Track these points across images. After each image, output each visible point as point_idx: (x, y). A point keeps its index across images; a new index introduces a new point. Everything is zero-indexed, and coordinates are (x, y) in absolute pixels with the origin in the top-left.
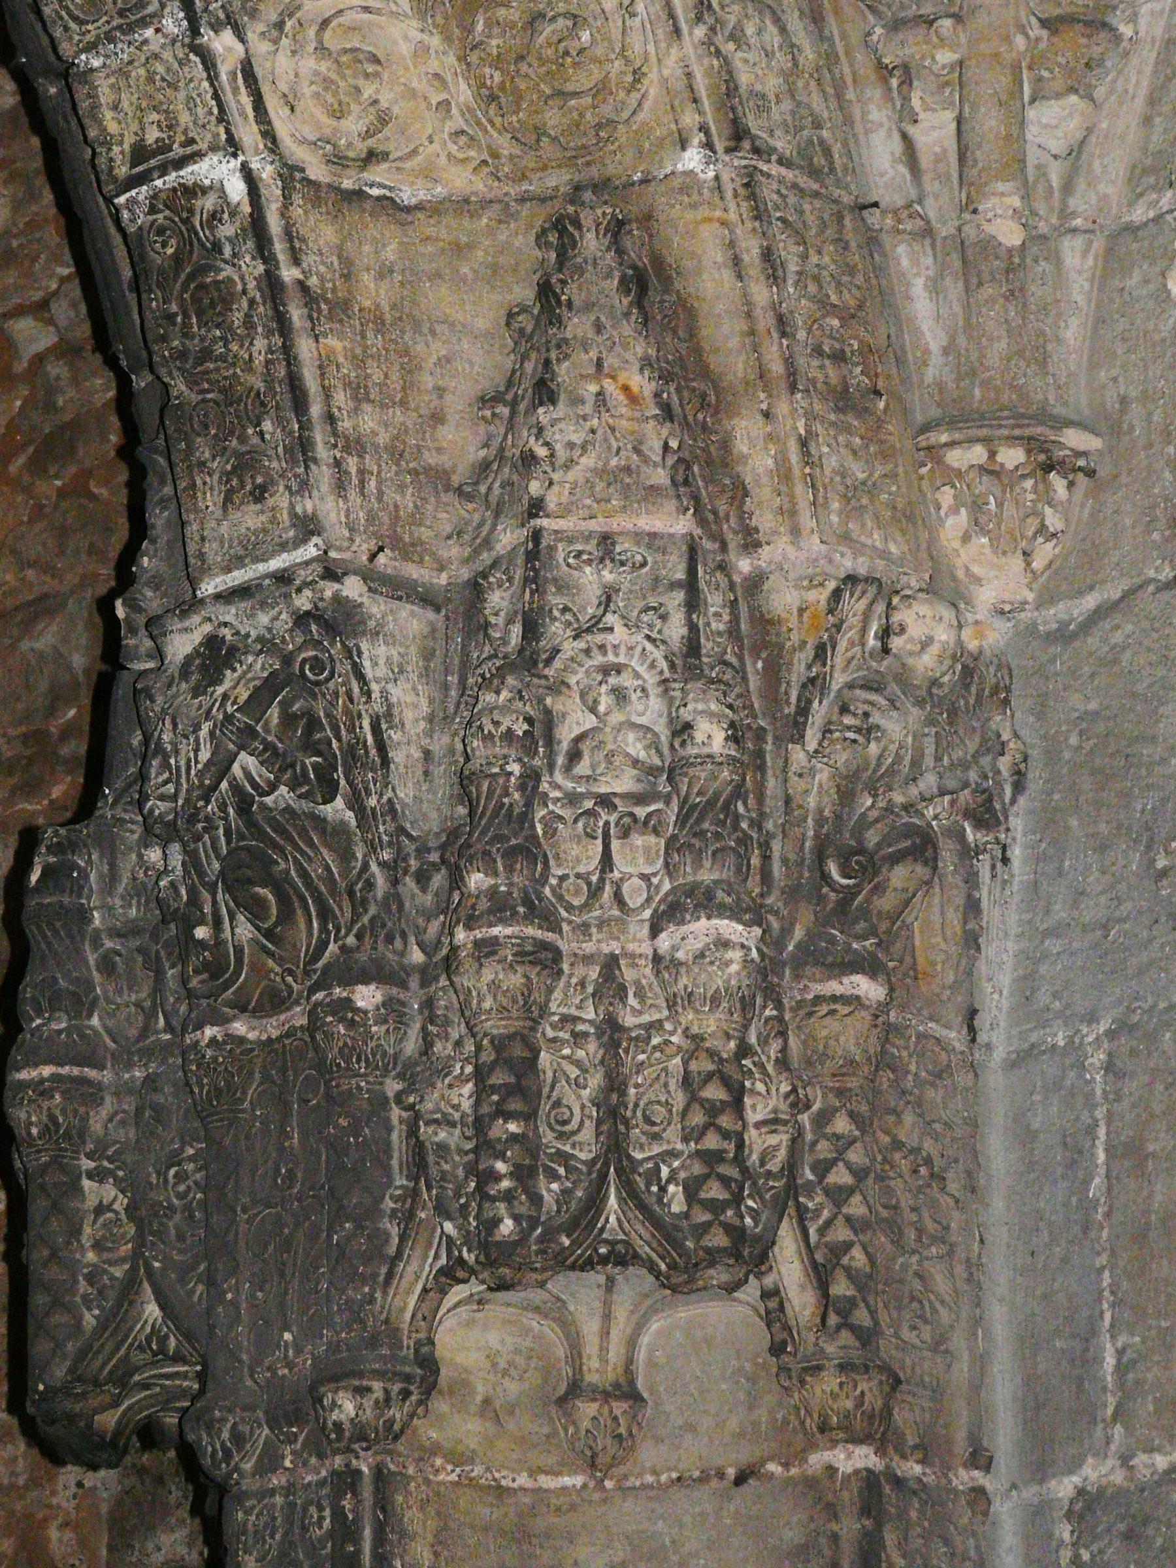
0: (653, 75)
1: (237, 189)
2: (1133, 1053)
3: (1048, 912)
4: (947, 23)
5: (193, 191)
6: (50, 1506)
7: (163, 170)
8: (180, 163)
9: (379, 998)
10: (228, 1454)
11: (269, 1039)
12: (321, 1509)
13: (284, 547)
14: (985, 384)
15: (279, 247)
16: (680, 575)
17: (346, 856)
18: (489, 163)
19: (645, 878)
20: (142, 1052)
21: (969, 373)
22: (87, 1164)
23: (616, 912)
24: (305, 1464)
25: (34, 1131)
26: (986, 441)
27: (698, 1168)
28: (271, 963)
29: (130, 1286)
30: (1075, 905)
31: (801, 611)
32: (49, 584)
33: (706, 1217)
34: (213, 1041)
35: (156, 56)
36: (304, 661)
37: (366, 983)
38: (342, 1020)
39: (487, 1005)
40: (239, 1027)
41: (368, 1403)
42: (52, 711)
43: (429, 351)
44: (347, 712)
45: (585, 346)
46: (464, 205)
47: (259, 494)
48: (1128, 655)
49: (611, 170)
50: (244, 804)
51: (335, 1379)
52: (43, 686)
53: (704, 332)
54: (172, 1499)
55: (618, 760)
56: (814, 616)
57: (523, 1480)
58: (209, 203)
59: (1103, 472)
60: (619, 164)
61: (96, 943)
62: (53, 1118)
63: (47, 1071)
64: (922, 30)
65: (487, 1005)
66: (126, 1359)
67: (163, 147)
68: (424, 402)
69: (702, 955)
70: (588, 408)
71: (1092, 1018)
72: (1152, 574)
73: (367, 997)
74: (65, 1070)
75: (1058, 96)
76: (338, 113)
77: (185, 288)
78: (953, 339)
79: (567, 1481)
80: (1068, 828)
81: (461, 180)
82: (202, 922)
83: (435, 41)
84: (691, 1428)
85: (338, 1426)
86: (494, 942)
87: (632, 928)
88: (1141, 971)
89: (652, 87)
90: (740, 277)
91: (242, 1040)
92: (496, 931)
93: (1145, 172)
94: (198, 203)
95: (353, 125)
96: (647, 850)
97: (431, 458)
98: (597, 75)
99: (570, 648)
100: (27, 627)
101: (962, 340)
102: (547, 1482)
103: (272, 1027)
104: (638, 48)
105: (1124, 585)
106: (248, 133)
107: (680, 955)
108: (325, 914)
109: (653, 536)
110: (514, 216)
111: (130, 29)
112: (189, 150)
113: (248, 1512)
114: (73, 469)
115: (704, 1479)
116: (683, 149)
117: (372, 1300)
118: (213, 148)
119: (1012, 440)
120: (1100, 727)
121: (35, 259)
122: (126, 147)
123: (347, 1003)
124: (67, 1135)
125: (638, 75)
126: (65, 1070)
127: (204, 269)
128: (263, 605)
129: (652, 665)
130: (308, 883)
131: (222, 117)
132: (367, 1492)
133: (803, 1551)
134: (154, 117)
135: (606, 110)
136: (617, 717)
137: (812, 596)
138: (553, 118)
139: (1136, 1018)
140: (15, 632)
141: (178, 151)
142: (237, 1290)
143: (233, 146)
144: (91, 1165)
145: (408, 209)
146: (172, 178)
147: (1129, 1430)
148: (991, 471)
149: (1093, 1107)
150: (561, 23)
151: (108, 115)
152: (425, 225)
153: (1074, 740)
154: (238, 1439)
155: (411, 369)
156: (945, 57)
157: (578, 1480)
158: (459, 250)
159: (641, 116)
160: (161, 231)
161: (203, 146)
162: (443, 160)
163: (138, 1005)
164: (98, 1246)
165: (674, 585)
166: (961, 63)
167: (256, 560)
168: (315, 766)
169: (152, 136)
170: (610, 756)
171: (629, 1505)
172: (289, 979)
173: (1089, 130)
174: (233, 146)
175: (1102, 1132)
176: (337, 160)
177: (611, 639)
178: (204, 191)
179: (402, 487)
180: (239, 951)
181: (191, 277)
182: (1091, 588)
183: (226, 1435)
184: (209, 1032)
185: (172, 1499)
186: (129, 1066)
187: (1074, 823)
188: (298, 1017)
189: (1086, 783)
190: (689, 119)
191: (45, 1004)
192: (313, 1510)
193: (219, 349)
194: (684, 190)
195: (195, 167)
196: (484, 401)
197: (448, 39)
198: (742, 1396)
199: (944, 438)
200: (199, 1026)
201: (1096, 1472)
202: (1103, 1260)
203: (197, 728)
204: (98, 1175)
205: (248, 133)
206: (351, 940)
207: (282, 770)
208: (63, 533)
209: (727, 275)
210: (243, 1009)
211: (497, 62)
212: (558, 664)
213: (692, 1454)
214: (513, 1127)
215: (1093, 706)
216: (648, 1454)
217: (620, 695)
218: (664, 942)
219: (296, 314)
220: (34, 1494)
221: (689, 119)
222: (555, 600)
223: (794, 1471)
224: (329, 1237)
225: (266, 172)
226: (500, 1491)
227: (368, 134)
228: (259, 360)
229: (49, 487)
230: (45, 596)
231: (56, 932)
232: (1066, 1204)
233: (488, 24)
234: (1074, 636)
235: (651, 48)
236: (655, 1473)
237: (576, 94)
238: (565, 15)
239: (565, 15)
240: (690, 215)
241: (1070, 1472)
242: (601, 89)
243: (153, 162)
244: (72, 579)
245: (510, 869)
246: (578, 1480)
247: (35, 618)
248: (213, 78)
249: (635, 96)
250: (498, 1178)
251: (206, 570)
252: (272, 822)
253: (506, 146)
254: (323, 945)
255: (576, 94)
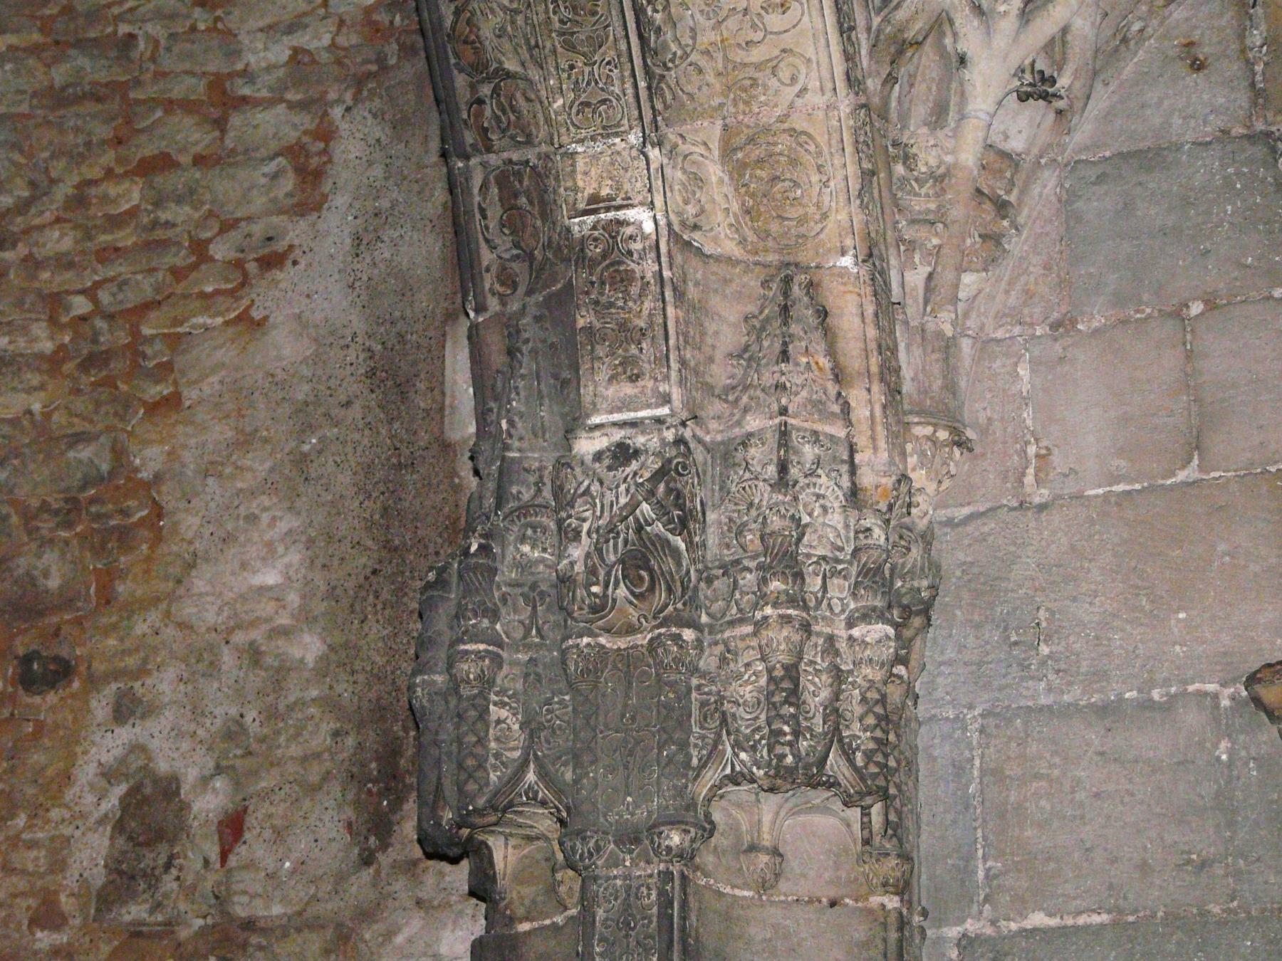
0: (832, 218)
1: (649, 227)
2: (997, 726)
3: (942, 653)
4: (941, 225)
5: (621, 223)
6: (60, 885)
7: (608, 209)
8: (618, 208)
9: (693, 637)
10: (591, 854)
11: (619, 649)
12: (649, 889)
13: (649, 406)
14: (932, 398)
15: (664, 259)
16: (845, 457)
17: (679, 564)
18: (742, 242)
19: (841, 600)
20: (524, 646)
21: (925, 392)
22: (493, 697)
23: (828, 614)
24: (637, 865)
25: (471, 676)
26: (935, 425)
27: (872, 745)
28: (631, 610)
29: (524, 765)
30: (959, 652)
31: (877, 487)
32: (88, 427)
33: (877, 770)
34: (588, 645)
35: (618, 153)
36: (678, 463)
37: (689, 627)
38: (676, 644)
39: (782, 648)
40: (602, 640)
41: (688, 838)
42: (83, 488)
43: (711, 327)
44: (691, 492)
45: (800, 339)
46: (730, 261)
47: (634, 379)
48: (992, 538)
49: (799, 259)
50: (639, 529)
51: (672, 823)
52: (79, 475)
53: (839, 345)
54: (141, 888)
55: (825, 540)
56: (885, 490)
57: (728, 890)
58: (629, 231)
59: (978, 450)
60: (805, 257)
61: (499, 588)
62: (482, 671)
63: (482, 647)
64: (928, 226)
65: (782, 648)
66: (512, 800)
67: (610, 198)
68: (706, 349)
69: (880, 641)
70: (802, 369)
71: (971, 707)
72: (1005, 502)
73: (688, 635)
74: (491, 648)
75: (977, 271)
76: (686, 202)
77: (607, 267)
78: (916, 374)
79: (746, 893)
80: (955, 615)
81: (731, 248)
82: (597, 584)
83: (726, 179)
84: (804, 876)
85: (669, 849)
86: (789, 616)
87: (837, 623)
88: (1000, 689)
89: (831, 224)
90: (863, 322)
91: (603, 647)
92: (790, 611)
93: (1005, 315)
94: (622, 230)
95: (691, 210)
96: (839, 586)
97: (709, 380)
98: (801, 211)
99: (803, 481)
100: (71, 446)
101: (921, 376)
102: (737, 892)
103: (622, 643)
104: (826, 203)
105: (988, 505)
106: (659, 202)
107: (868, 639)
108: (670, 591)
109: (832, 436)
110: (752, 271)
111: (608, 136)
112: (625, 202)
113: (600, 886)
114: (104, 373)
115: (810, 902)
116: (843, 255)
117: (686, 787)
118: (642, 204)
119: (947, 427)
120: (976, 570)
121: (85, 269)
122: (586, 194)
123: (679, 636)
124: (488, 681)
125: (825, 216)
126: (491, 648)
127: (620, 263)
128: (643, 433)
129: (837, 497)
130: (663, 574)
131: (650, 190)
132: (677, 882)
133: (866, 945)
134: (610, 182)
135: (802, 230)
136: (821, 520)
137: (884, 480)
138: (775, 227)
139: (998, 710)
140: (63, 447)
141: (619, 202)
142: (596, 772)
143: (652, 206)
144: (496, 698)
145: (708, 257)
146: (611, 215)
147: (994, 908)
148: (932, 439)
149: (972, 749)
150: (787, 184)
151: (579, 177)
152: (714, 267)
153: (958, 573)
154: (598, 849)
155: (703, 334)
156: (935, 241)
157: (751, 894)
158: (726, 282)
159: (822, 236)
160: (596, 239)
161: (636, 202)
162: (722, 236)
163: (521, 622)
164: (497, 740)
165: (843, 462)
166: (940, 247)
167: (629, 410)
168: (678, 516)
169: (605, 192)
170: (820, 537)
171: (773, 910)
172: (643, 620)
173: (980, 291)
174: (652, 206)
175: (977, 762)
176: (683, 224)
177: (819, 481)
178: (628, 224)
179: (697, 390)
180: (614, 600)
181: (612, 264)
182: (969, 504)
183: (591, 844)
184: (586, 640)
185: (141, 888)
186: (518, 651)
187: (958, 613)
188: (642, 639)
189: (966, 596)
190: (849, 242)
191: (480, 613)
192: (644, 889)
193: (620, 303)
194: (841, 275)
195: (627, 212)
196: (731, 355)
197: (732, 178)
198: (831, 863)
199: (916, 420)
200: (581, 637)
201: (971, 926)
202: (976, 824)
203: (617, 486)
204: (502, 705)
205: (659, 202)
206: (680, 606)
207: (664, 515)
208: (98, 404)
209: (857, 320)
210: (608, 631)
211: (752, 195)
212: (797, 488)
213: (804, 889)
214: (792, 710)
215: (969, 559)
216: (783, 886)
217: (825, 509)
218: (856, 632)
219: (668, 294)
220: (48, 878)
221: (849, 242)
222: (794, 458)
223: (860, 904)
224: (660, 752)
225: (662, 222)
226: (720, 894)
227: (697, 216)
228: (645, 313)
229: (86, 380)
230: (83, 433)
231: (483, 576)
232: (954, 794)
233: (751, 176)
234: (958, 525)
235: (833, 204)
236: (786, 895)
237: (788, 219)
238: (791, 180)
239: (791, 180)
240: (842, 288)
241: (956, 925)
242: (802, 220)
243: (601, 205)
244: (100, 426)
245: (794, 583)
246: (751, 894)
247: (77, 442)
248: (648, 169)
249: (820, 226)
250: (785, 734)
251: (595, 410)
252: (650, 539)
253: (751, 237)
254: (666, 606)
255: (788, 219)
